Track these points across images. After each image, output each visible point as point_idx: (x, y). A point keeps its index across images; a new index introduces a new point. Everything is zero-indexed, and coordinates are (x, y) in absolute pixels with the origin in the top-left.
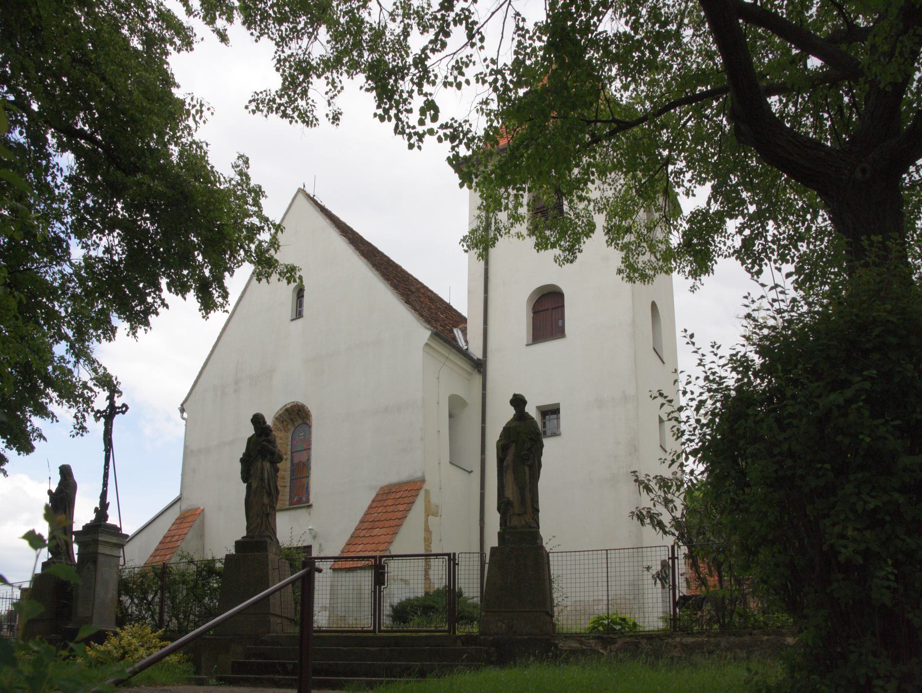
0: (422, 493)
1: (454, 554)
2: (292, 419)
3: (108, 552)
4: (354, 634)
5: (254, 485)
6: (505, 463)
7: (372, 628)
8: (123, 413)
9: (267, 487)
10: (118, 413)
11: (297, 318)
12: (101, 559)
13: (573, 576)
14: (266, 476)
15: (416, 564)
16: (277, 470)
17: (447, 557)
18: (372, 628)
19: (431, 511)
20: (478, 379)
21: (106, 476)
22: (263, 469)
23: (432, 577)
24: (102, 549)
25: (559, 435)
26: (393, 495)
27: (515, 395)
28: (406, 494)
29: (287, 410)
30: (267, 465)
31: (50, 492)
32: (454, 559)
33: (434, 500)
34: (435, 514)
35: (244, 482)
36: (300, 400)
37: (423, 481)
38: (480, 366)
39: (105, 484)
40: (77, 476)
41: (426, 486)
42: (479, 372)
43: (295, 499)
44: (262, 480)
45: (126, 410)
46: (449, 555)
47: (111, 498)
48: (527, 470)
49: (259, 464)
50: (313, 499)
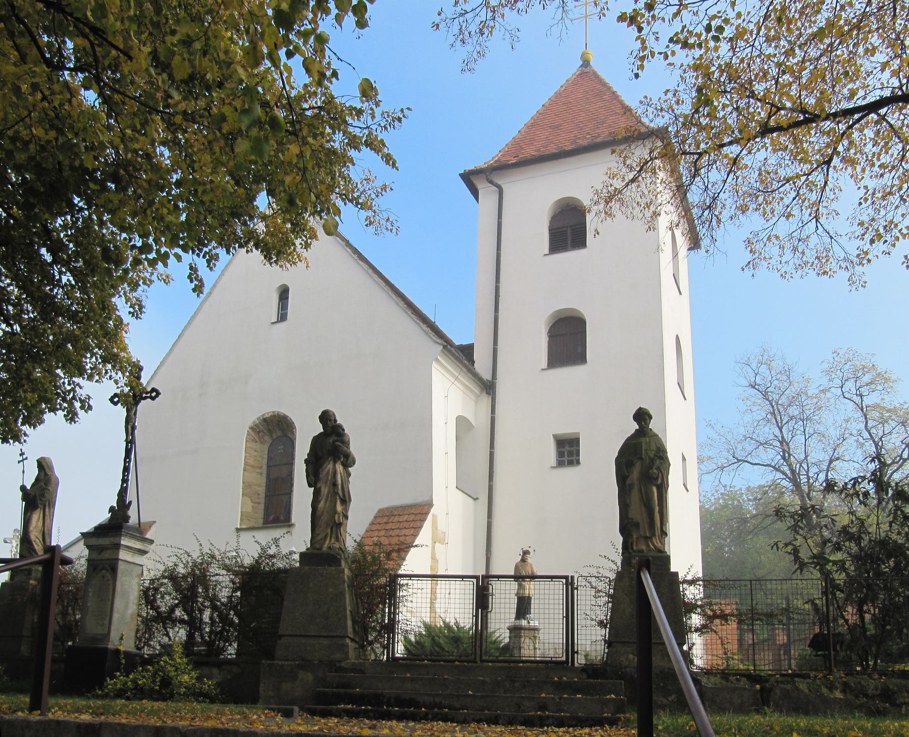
0: (430, 517)
1: (572, 577)
2: (269, 431)
3: (130, 560)
4: (506, 665)
5: (325, 490)
6: (628, 481)
7: (564, 659)
8: (153, 398)
9: (340, 493)
10: (145, 398)
11: (278, 322)
12: (121, 566)
13: (546, 616)
14: (339, 481)
15: (508, 587)
16: (349, 475)
17: (564, 581)
18: (564, 659)
19: (438, 538)
20: (486, 401)
21: (126, 469)
22: (335, 472)
23: (438, 610)
24: (123, 555)
25: (578, 463)
26: (396, 519)
27: (640, 409)
28: (412, 517)
29: (265, 420)
30: (339, 468)
31: (23, 488)
32: (572, 583)
33: (441, 526)
34: (443, 542)
35: (310, 485)
36: (284, 410)
37: (430, 505)
38: (489, 387)
39: (125, 480)
40: (59, 471)
41: (433, 511)
42: (488, 393)
43: (271, 518)
44: (335, 484)
45: (157, 396)
46: (566, 577)
47: (131, 496)
48: (655, 489)
49: (330, 466)
50: (293, 521)
